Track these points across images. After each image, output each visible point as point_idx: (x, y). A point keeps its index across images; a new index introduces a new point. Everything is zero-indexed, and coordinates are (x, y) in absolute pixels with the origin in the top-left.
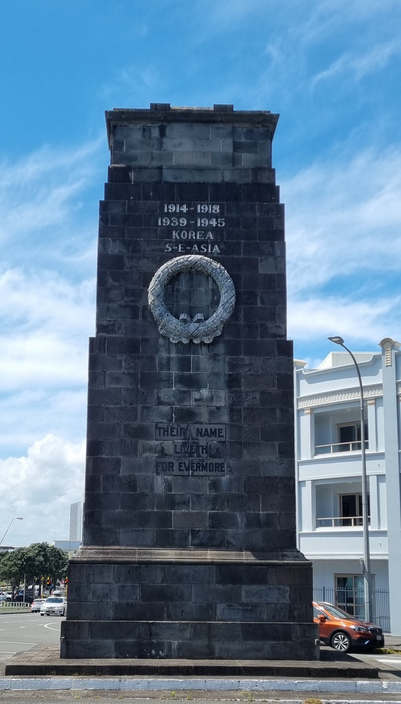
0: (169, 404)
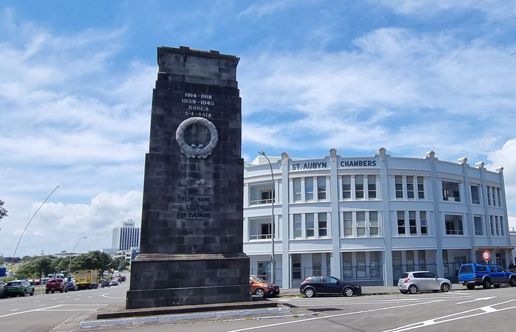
0: (184, 186)
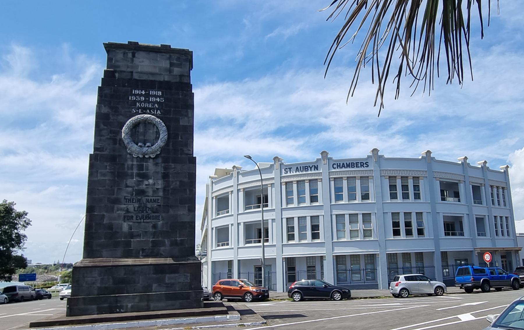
0: (131, 187)
